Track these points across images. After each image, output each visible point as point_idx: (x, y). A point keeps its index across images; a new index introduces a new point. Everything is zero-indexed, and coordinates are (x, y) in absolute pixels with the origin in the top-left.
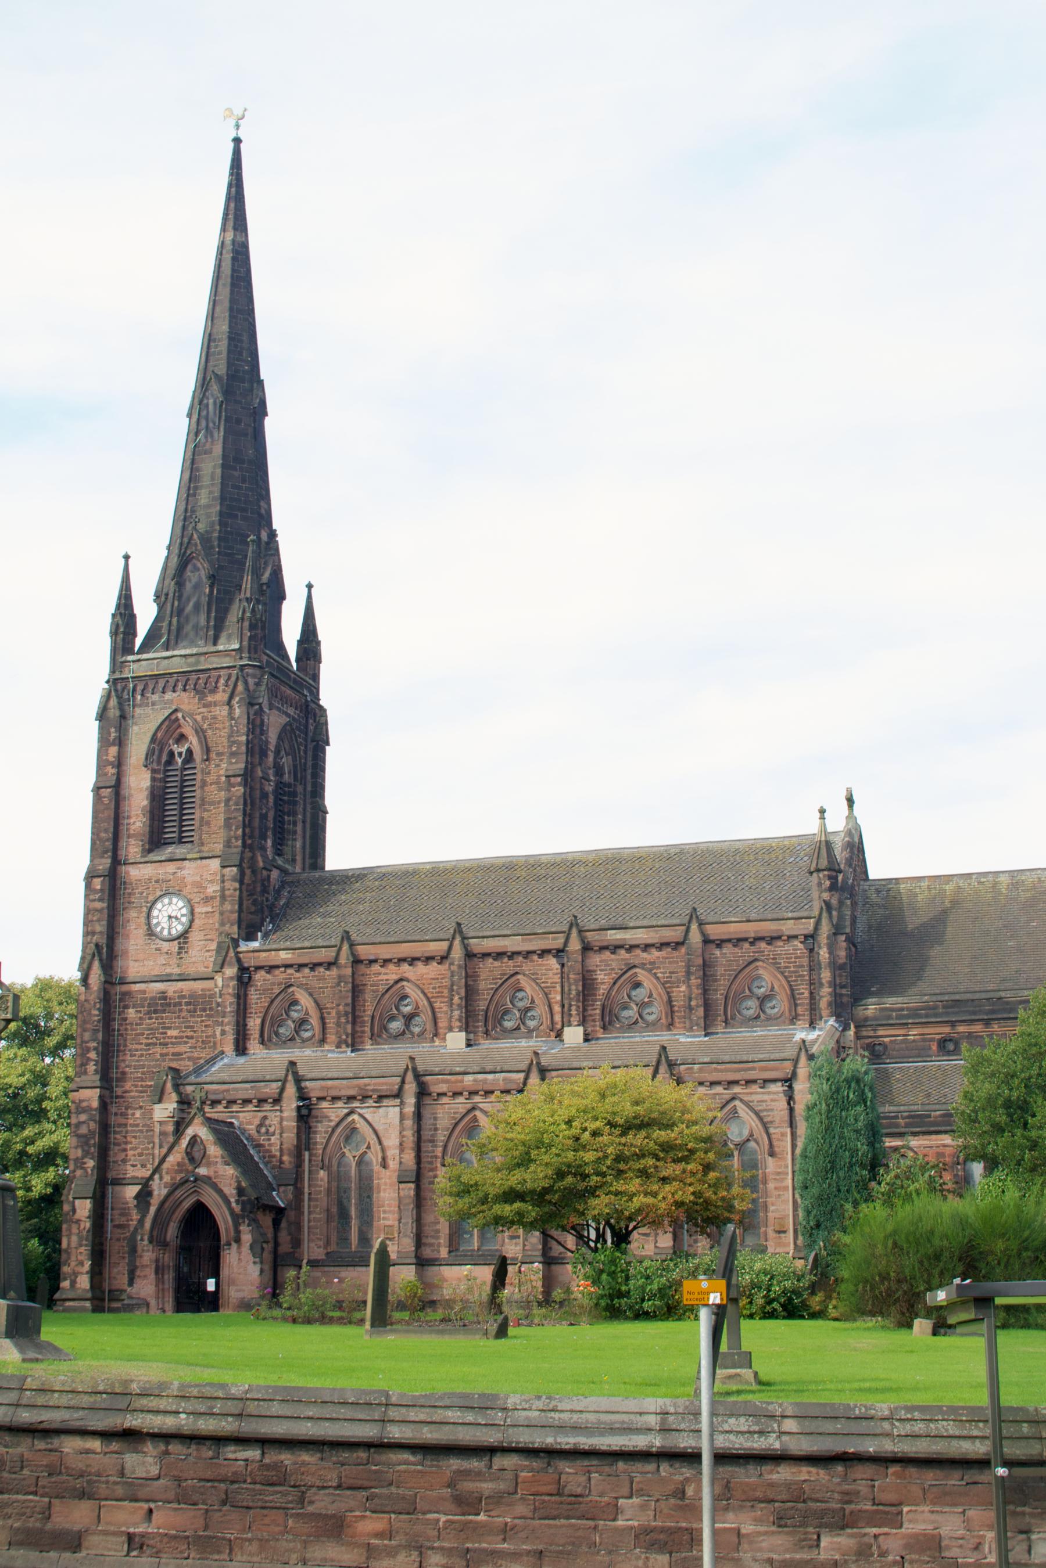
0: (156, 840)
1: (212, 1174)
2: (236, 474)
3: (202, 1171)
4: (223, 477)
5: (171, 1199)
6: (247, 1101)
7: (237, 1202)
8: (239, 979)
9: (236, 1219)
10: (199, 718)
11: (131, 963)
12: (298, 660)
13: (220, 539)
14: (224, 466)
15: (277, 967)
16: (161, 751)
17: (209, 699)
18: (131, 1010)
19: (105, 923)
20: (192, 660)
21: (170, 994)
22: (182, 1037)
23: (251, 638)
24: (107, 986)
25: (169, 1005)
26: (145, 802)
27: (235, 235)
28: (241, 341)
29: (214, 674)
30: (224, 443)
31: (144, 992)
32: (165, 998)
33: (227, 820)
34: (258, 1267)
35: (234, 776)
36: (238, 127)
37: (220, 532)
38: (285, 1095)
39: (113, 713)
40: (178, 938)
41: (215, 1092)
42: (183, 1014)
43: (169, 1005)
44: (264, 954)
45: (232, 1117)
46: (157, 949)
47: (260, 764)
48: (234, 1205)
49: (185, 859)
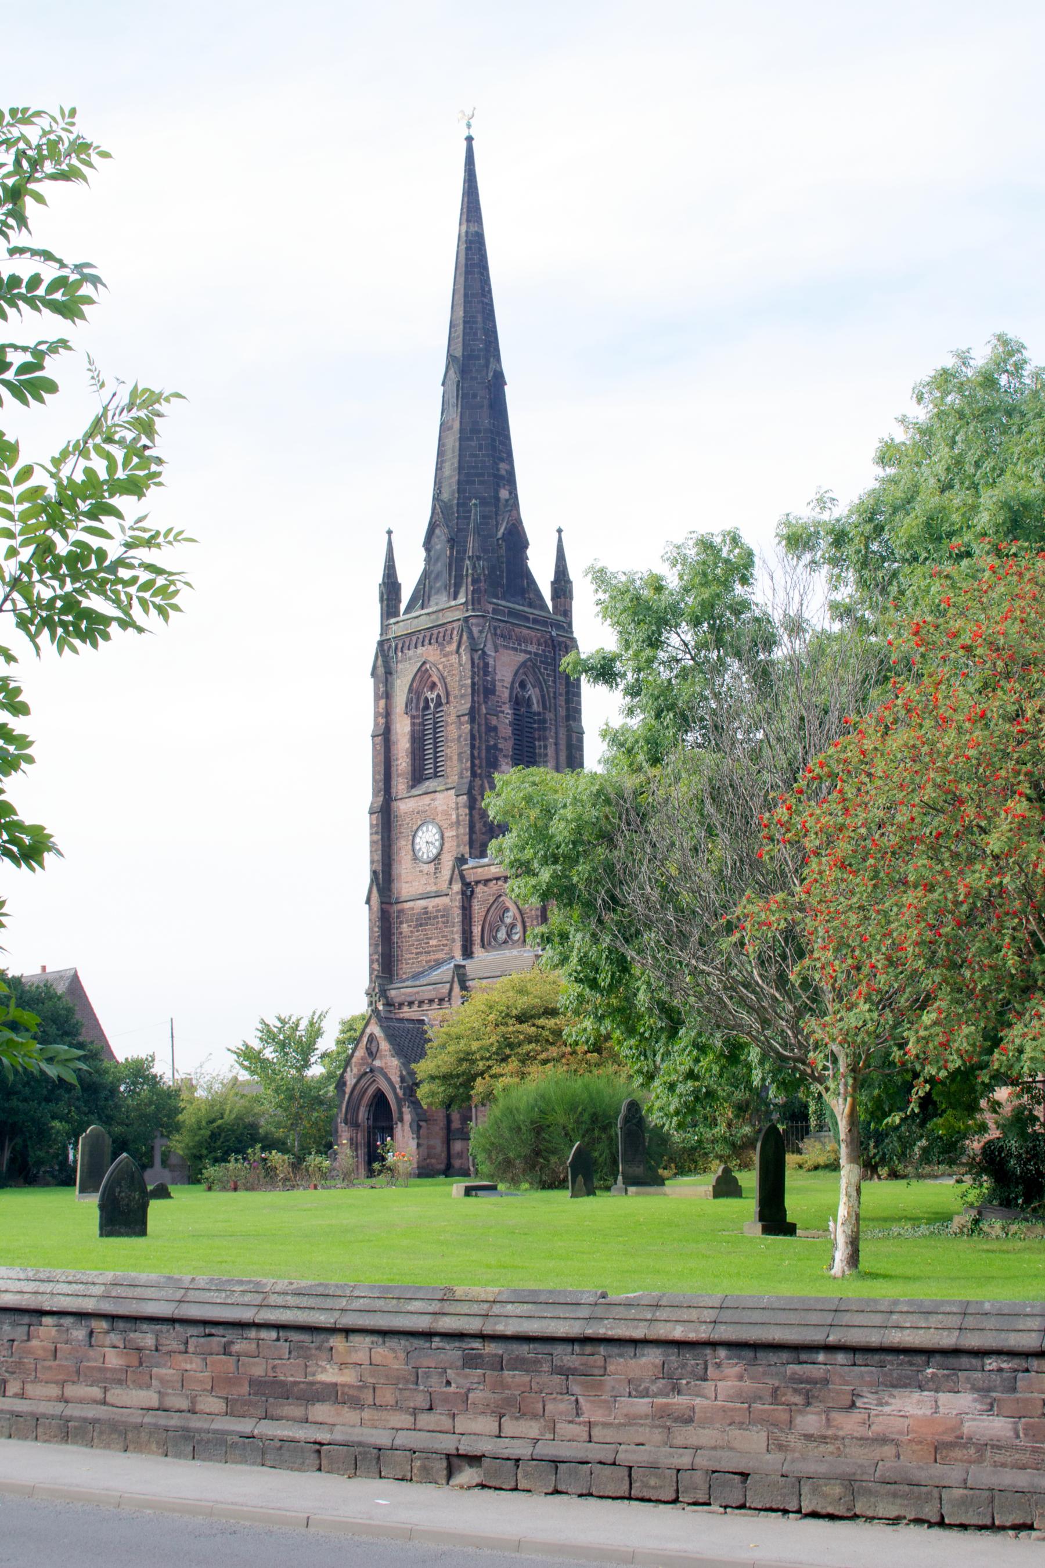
0: (418, 777)
1: (383, 1065)
2: (473, 444)
3: (377, 1063)
4: (461, 449)
5: (358, 1087)
6: (431, 1001)
7: (400, 1087)
8: (463, 893)
9: (399, 1101)
10: (440, 667)
11: (404, 885)
12: (553, 599)
13: (458, 504)
14: (461, 439)
15: (490, 880)
16: (418, 700)
17: (447, 649)
18: (405, 925)
19: (380, 852)
20: (433, 617)
21: (430, 909)
22: (439, 946)
23: (473, 592)
24: (384, 906)
25: (429, 918)
26: (408, 745)
27: (468, 227)
28: (476, 322)
29: (449, 627)
30: (461, 418)
31: (412, 909)
32: (426, 913)
33: (460, 754)
34: (415, 1142)
35: (463, 715)
36: (469, 126)
37: (458, 499)
38: (453, 994)
39: (381, 670)
40: (434, 860)
41: (410, 995)
42: (440, 925)
43: (429, 918)
44: (480, 870)
45: (423, 1015)
46: (421, 871)
47: (486, 702)
48: (398, 1090)
49: (435, 792)
